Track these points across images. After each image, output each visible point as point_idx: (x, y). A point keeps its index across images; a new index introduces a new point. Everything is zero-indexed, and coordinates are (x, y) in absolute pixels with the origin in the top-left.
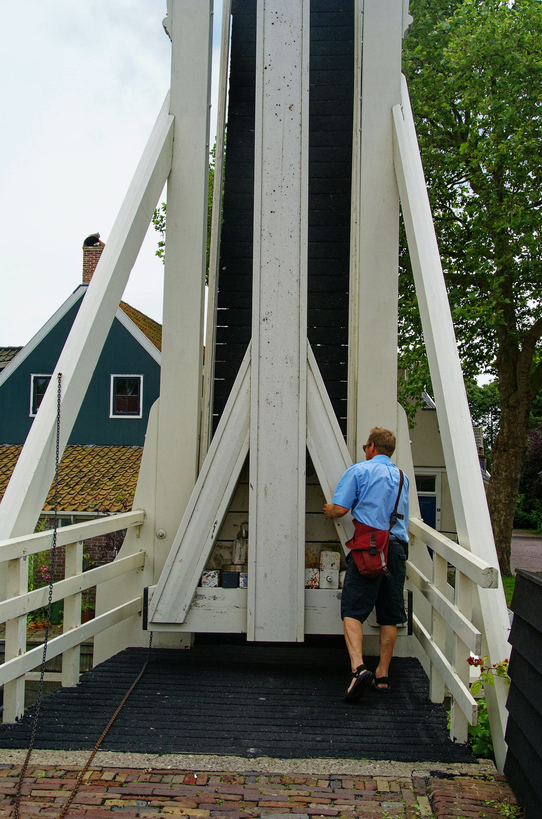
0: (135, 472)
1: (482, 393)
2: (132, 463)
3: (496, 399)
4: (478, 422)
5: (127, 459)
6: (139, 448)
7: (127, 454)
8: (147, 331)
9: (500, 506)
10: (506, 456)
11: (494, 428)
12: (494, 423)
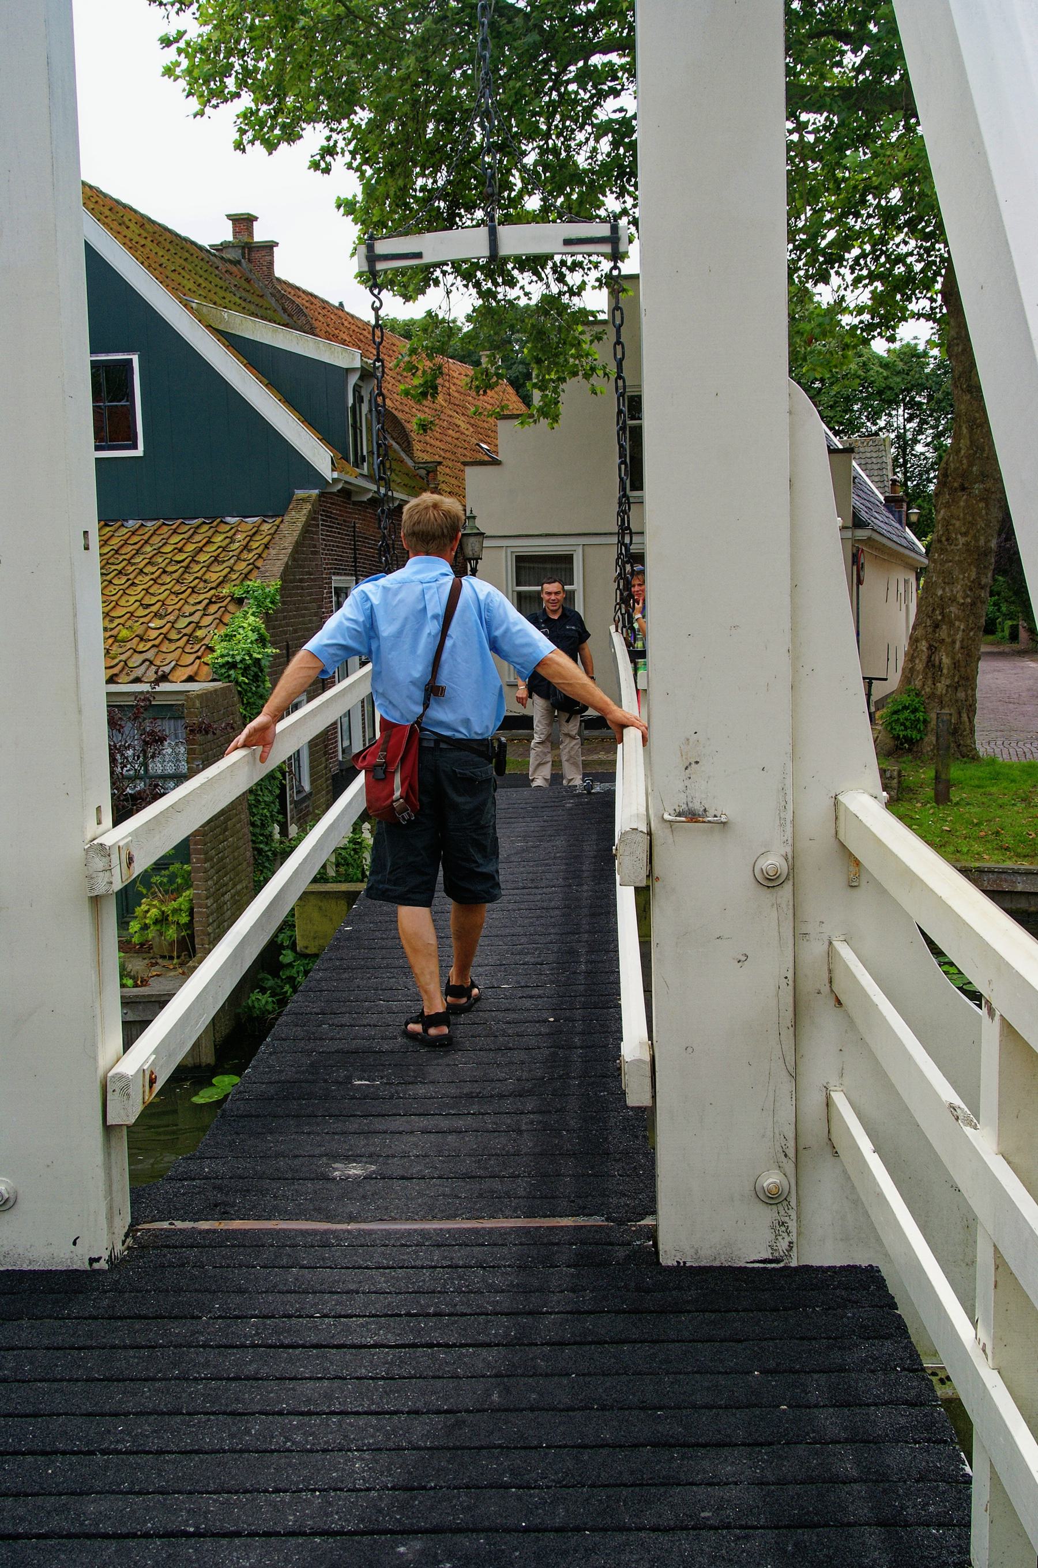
0: (130, 582)
1: (885, 366)
2: (125, 563)
3: (913, 377)
4: (876, 424)
5: (113, 552)
6: (142, 525)
7: (113, 542)
8: (146, 251)
9: (954, 609)
10: (967, 501)
11: (909, 435)
12: (908, 426)
